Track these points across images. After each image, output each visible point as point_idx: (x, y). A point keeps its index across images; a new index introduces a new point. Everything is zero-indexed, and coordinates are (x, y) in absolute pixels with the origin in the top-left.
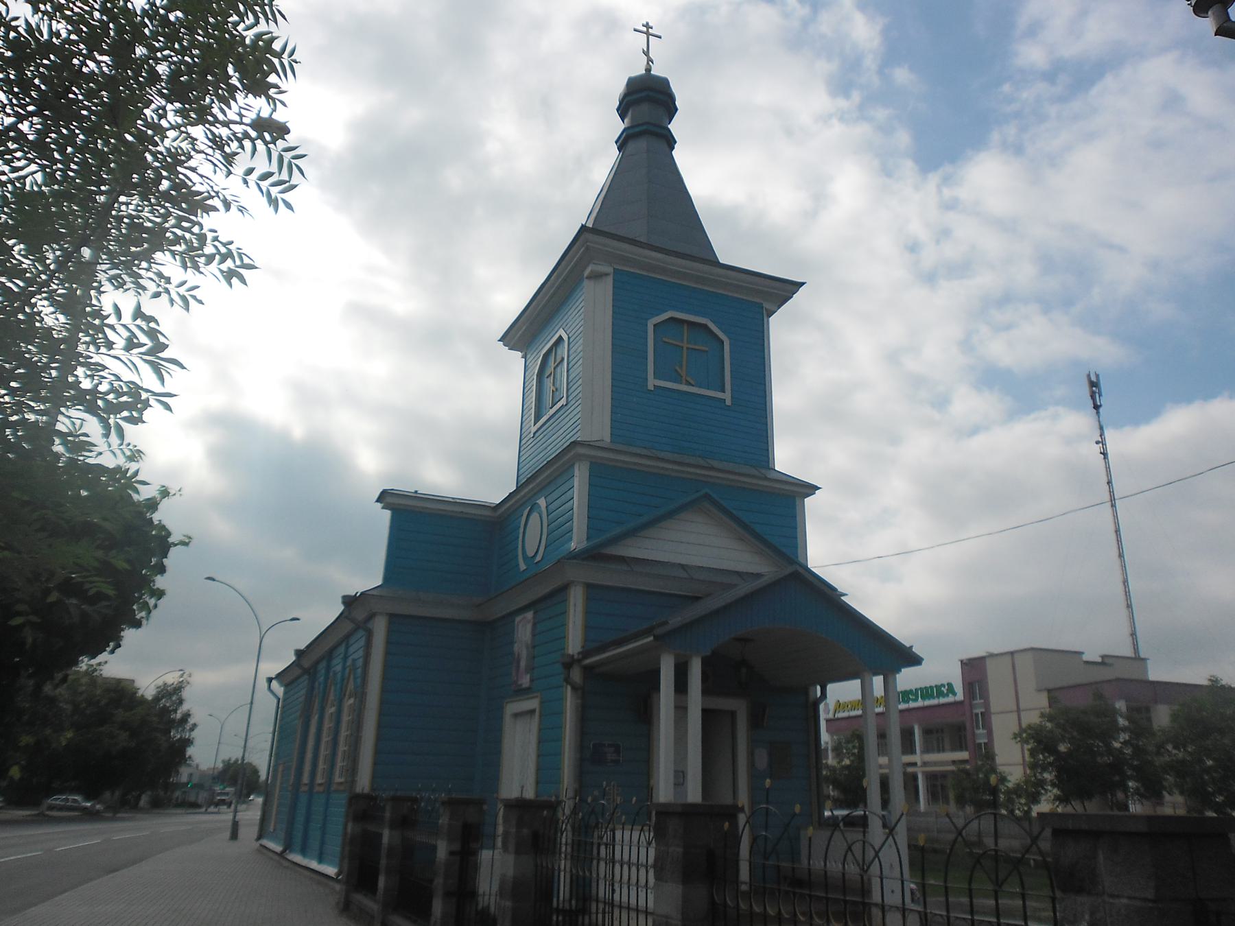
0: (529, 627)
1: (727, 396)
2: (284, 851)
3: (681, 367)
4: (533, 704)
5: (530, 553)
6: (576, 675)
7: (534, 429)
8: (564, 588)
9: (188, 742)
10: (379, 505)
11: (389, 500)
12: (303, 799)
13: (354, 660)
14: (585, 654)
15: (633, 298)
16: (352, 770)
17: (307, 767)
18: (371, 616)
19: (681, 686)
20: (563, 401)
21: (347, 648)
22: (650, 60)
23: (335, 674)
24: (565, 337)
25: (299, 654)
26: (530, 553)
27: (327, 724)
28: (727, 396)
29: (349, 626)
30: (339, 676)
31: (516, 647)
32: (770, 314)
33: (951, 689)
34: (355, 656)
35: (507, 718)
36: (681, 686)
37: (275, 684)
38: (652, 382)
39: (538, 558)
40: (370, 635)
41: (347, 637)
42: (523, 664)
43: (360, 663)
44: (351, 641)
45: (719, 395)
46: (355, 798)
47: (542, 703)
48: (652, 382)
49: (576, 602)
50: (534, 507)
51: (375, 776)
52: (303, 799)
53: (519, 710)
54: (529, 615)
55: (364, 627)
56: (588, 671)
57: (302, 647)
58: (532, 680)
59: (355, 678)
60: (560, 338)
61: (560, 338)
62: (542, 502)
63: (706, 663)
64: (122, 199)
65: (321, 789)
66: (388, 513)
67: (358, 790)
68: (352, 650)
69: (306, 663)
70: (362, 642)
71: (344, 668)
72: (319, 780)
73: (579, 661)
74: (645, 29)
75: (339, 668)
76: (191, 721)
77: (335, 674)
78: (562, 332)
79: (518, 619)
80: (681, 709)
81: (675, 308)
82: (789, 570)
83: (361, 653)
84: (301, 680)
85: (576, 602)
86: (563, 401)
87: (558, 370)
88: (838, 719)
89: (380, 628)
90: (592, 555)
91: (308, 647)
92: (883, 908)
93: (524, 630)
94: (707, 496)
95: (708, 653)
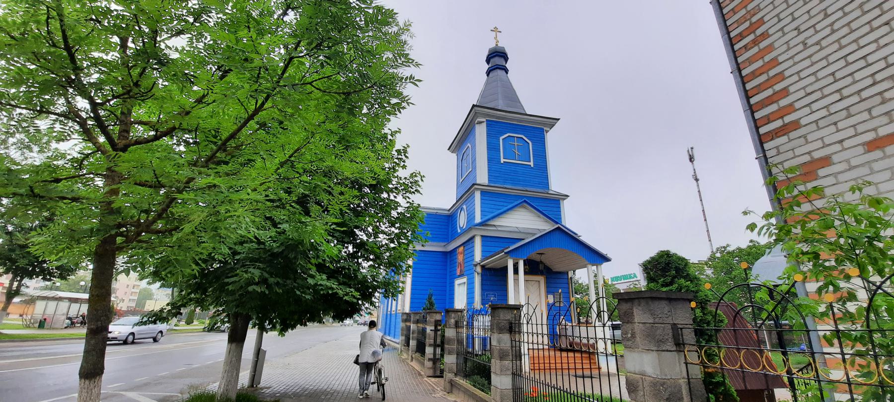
1: (532, 164)
6: (479, 269)
8: (473, 238)
9: (320, 321)
15: (495, 128)
16: (403, 306)
19: (516, 271)
28: (532, 164)
32: (547, 132)
33: (635, 276)
35: (456, 287)
36: (516, 271)
38: (502, 160)
48: (502, 160)
49: (478, 242)
51: (411, 307)
56: (483, 267)
62: (464, 207)
64: (197, 7)
80: (516, 280)
82: (557, 226)
85: (478, 242)
90: (483, 224)
94: (525, 201)
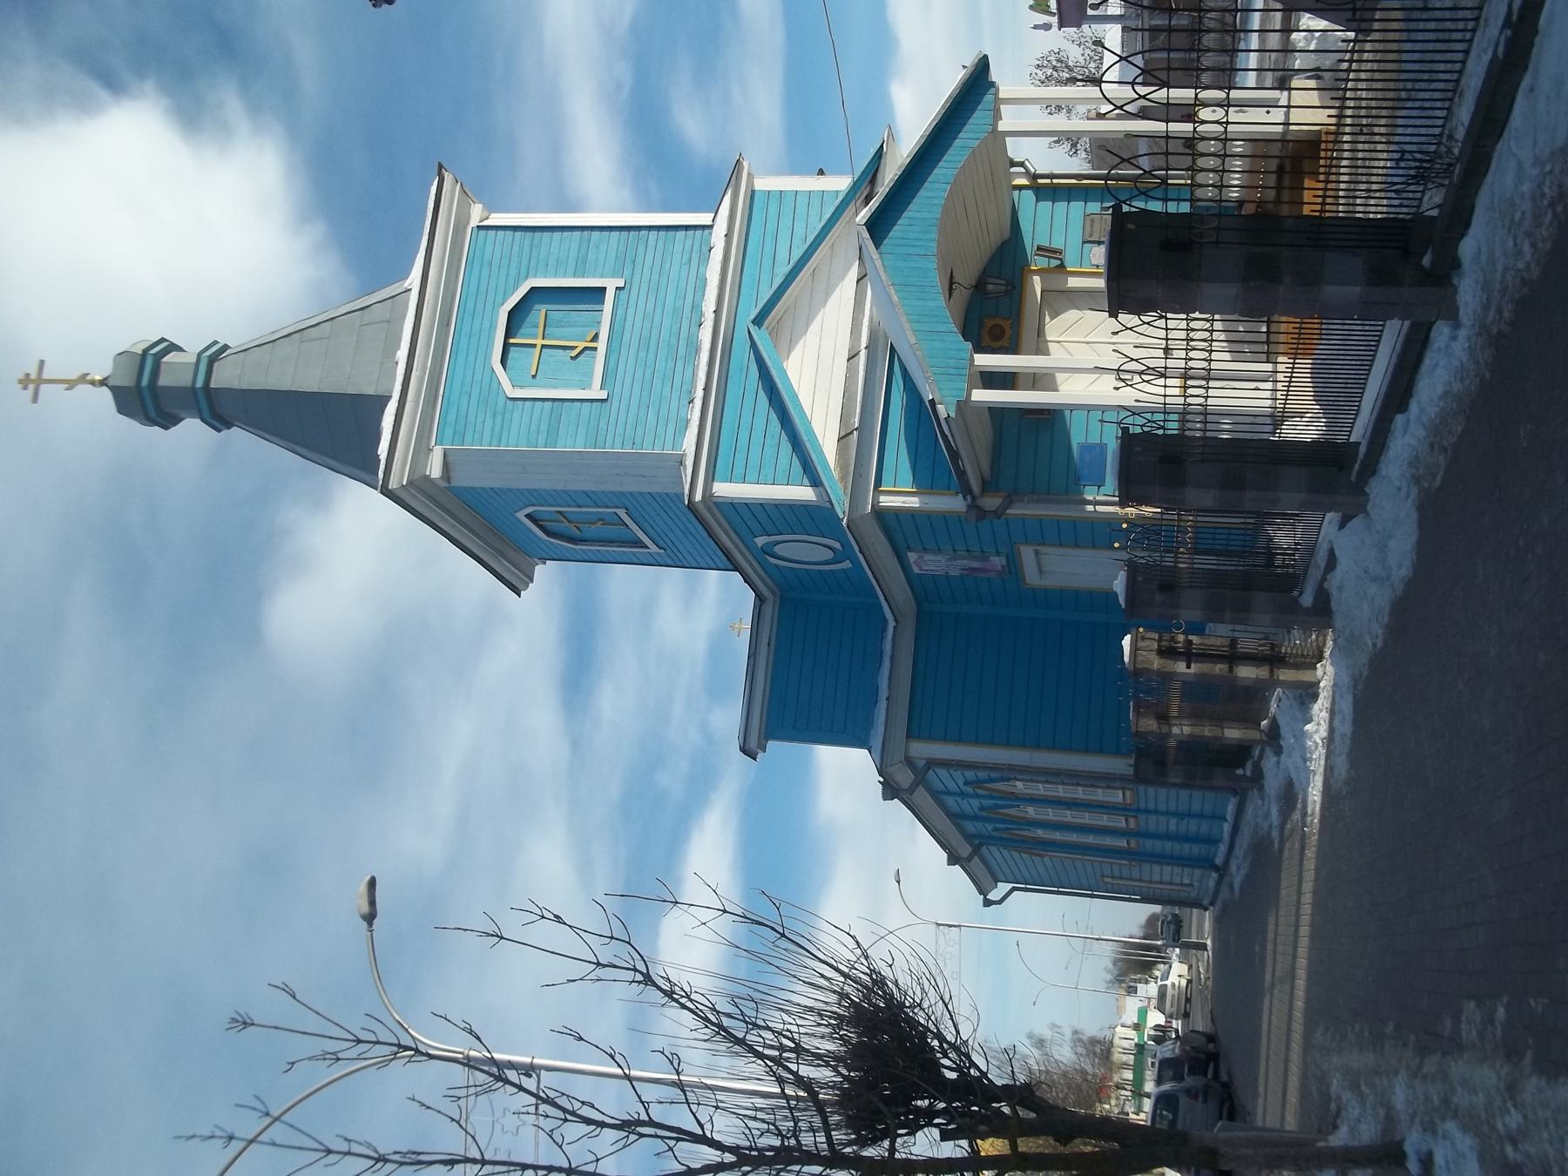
0: (928, 557)
2: (1216, 868)
3: (574, 348)
4: (1027, 553)
5: (829, 555)
6: (991, 502)
7: (653, 548)
10: (760, 756)
11: (753, 743)
12: (1149, 844)
13: (967, 783)
14: (966, 490)
16: (1108, 780)
17: (1108, 841)
18: (909, 762)
20: (622, 513)
21: (949, 793)
22: (83, 379)
23: (982, 808)
24: (529, 510)
25: (953, 859)
26: (829, 555)
27: (1051, 814)
29: (921, 795)
30: (986, 802)
31: (954, 573)
34: (961, 782)
37: (992, 896)
39: (837, 545)
40: (932, 763)
41: (936, 795)
42: (976, 564)
43: (970, 775)
44: (941, 787)
45: (610, 296)
46: (1140, 778)
47: (1027, 543)
50: (767, 551)
52: (1149, 844)
53: (1036, 571)
54: (912, 557)
55: (922, 772)
56: (986, 487)
57: (943, 856)
58: (998, 553)
59: (991, 780)
60: (528, 516)
61: (528, 516)
63: (980, 349)
65: (1132, 821)
66: (771, 744)
67: (1131, 771)
68: (952, 786)
69: (965, 850)
70: (943, 772)
71: (977, 796)
72: (1120, 823)
73: (974, 498)
74: (31, 387)
75: (975, 803)
76: (1047, 1034)
77: (982, 808)
78: (521, 515)
79: (916, 570)
81: (488, 357)
83: (957, 774)
84: (989, 857)
86: (622, 513)
87: (572, 518)
88: (1059, 8)
89: (923, 750)
91: (944, 847)
92: (1287, 124)
93: (931, 564)
95: (969, 345)
